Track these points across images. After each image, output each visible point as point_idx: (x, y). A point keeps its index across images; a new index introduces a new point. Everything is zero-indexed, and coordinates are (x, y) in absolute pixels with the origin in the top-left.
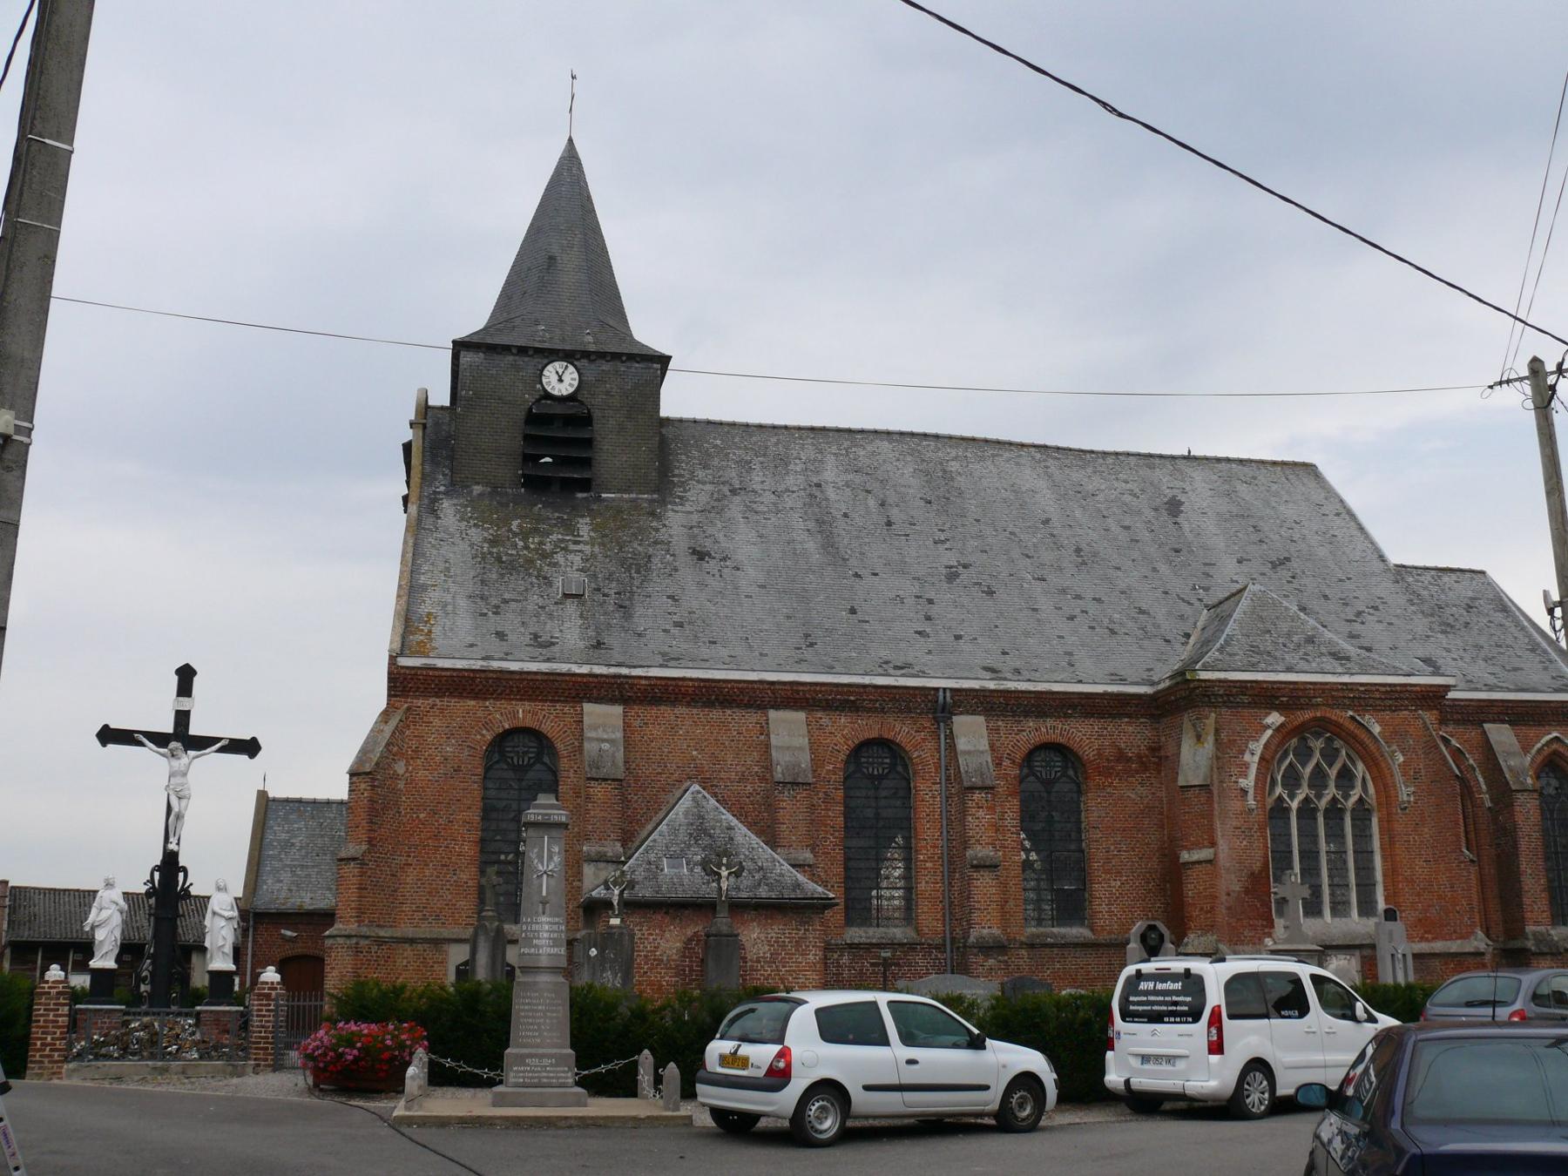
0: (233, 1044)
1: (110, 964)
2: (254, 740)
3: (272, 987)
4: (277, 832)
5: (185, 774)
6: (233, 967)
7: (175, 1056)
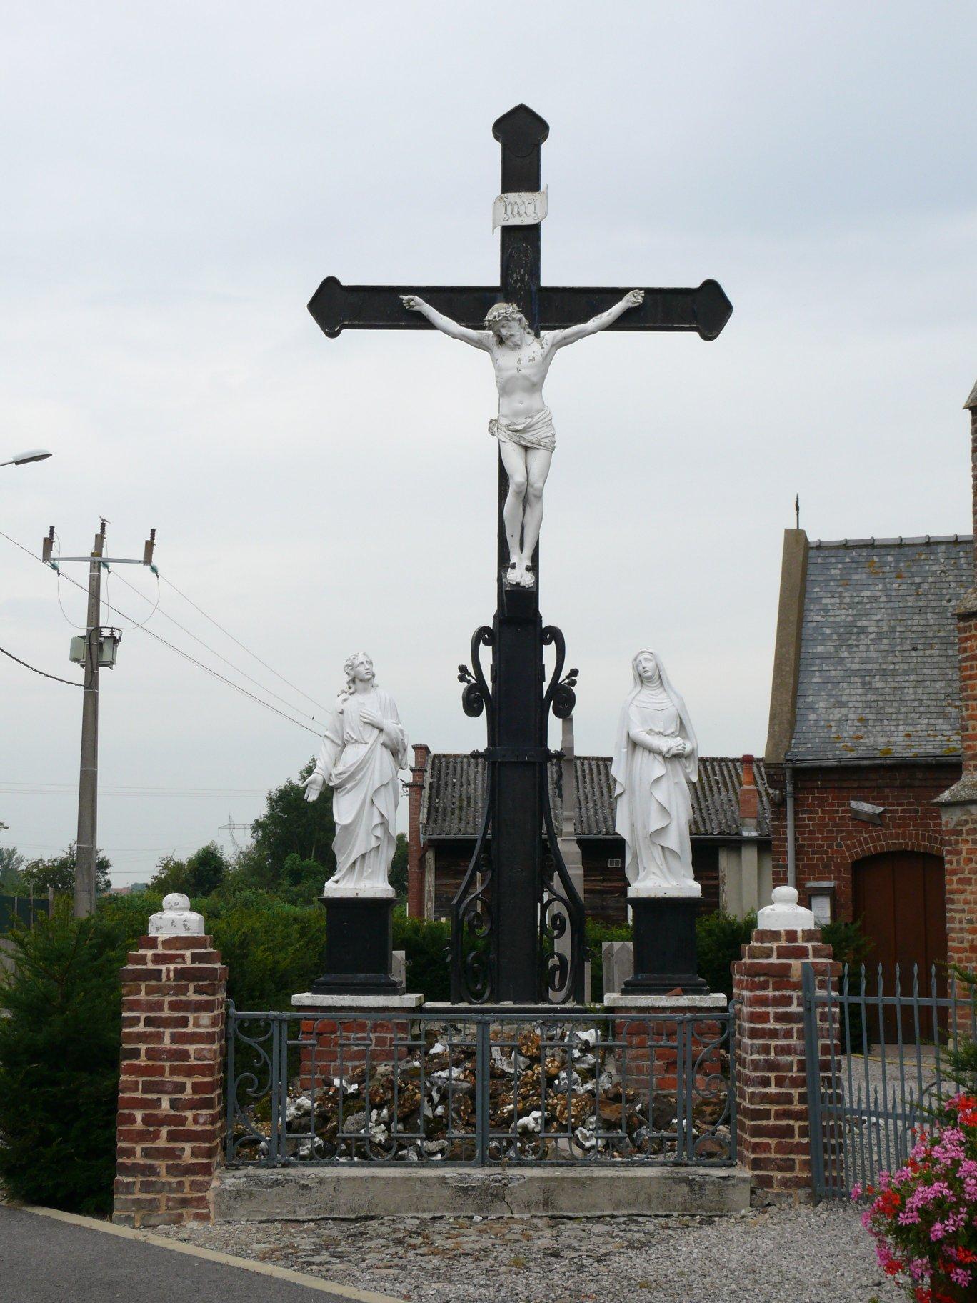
0: (690, 1120)
1: (375, 885)
2: (711, 287)
3: (791, 944)
4: (829, 608)
5: (535, 386)
6: (693, 888)
7: (533, 1148)
